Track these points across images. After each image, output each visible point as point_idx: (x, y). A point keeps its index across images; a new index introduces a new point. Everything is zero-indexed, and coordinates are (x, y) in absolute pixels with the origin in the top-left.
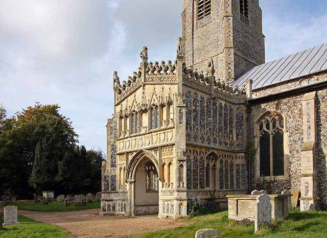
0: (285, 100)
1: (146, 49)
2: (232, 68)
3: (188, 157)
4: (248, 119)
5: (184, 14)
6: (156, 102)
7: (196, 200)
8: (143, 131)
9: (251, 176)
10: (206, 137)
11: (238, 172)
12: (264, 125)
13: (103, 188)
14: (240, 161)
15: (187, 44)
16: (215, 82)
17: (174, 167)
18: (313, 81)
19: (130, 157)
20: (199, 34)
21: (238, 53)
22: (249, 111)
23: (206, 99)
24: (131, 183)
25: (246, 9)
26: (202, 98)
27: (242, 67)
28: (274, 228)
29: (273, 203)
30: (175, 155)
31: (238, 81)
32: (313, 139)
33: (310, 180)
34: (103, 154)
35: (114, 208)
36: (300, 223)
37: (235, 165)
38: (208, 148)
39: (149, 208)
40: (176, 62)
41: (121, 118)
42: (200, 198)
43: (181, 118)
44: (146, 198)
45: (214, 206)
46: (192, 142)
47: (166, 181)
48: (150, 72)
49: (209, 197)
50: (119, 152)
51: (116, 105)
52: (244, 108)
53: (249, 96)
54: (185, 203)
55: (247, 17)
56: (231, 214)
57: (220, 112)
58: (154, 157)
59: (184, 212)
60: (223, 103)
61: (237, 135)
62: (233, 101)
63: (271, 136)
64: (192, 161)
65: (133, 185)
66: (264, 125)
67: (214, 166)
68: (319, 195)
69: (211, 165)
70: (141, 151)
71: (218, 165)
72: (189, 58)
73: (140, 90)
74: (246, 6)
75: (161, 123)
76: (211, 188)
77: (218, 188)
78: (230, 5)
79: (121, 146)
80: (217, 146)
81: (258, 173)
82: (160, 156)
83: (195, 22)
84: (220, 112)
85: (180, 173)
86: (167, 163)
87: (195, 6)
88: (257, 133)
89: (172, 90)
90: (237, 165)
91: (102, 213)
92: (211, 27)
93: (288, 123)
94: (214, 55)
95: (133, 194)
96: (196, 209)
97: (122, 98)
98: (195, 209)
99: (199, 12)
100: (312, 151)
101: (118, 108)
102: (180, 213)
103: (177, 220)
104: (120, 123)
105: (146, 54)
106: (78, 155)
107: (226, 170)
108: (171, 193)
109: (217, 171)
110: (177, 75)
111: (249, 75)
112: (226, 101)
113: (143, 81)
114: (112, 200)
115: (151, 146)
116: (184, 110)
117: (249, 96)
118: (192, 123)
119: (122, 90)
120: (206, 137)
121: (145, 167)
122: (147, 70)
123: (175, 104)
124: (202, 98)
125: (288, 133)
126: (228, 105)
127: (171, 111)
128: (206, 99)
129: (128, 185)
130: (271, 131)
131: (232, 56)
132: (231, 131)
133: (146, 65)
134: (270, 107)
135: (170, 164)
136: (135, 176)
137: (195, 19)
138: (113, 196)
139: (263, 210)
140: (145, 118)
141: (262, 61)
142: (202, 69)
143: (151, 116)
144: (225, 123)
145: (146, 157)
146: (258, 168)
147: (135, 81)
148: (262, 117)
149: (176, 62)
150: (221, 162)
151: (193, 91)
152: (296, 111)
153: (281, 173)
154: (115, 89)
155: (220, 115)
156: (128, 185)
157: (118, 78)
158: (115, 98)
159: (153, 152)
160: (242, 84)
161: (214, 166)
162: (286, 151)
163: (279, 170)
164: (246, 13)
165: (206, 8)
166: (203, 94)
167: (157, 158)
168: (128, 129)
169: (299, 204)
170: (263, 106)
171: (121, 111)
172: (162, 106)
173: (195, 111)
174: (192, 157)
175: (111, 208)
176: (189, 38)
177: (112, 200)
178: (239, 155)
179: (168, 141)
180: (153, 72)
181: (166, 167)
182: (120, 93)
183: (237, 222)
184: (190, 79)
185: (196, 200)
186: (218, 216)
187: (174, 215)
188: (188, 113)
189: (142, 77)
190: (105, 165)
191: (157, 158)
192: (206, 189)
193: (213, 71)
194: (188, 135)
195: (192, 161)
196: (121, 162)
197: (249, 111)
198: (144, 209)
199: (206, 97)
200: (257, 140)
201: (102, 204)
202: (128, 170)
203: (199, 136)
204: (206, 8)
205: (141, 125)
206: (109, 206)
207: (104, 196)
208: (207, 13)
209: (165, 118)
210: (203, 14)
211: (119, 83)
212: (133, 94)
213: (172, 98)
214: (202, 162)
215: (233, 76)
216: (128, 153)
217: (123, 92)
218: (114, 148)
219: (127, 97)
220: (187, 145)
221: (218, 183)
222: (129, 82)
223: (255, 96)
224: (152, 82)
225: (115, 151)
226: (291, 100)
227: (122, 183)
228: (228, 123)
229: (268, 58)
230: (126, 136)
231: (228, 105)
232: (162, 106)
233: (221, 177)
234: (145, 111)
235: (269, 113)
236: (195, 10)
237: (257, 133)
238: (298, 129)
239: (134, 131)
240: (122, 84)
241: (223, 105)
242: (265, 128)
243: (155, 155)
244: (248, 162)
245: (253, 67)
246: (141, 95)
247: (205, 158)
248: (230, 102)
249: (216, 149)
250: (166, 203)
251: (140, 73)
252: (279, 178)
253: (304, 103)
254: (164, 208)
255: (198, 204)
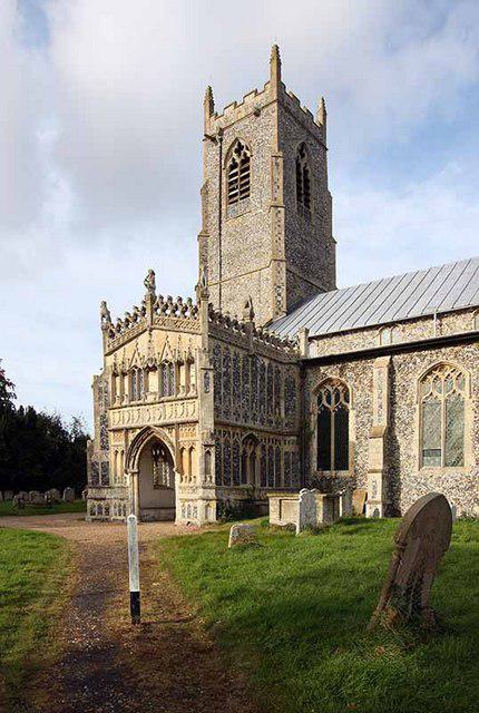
0: (352, 365)
1: (153, 273)
2: (284, 294)
3: (218, 439)
4: (302, 386)
5: (205, 191)
6: (170, 357)
7: (228, 500)
8: (150, 399)
9: (305, 470)
10: (241, 412)
11: (286, 463)
12: (324, 398)
13: (90, 481)
14: (289, 447)
15: (210, 244)
16: (254, 331)
17: (198, 454)
18: (386, 339)
19: (131, 437)
20: (231, 230)
21: (293, 268)
22: (303, 376)
23: (241, 356)
24: (133, 474)
25: (307, 194)
26: (237, 355)
27: (299, 292)
28: (317, 531)
29: (321, 504)
30: (198, 437)
31: (292, 316)
32: (384, 423)
33: (378, 477)
34: (62, 420)
35: (107, 510)
36: (351, 528)
37: (282, 453)
38: (245, 429)
39: (159, 508)
40: (199, 302)
41: (115, 375)
42: (233, 498)
43: (207, 385)
44: (155, 497)
45: (253, 508)
46: (223, 419)
47: (186, 474)
48: (159, 311)
49: (246, 497)
50: (113, 427)
51: (106, 355)
52: (296, 370)
53: (303, 354)
54: (214, 504)
55: (309, 207)
56: (273, 518)
57: (262, 376)
58: (169, 438)
59: (212, 517)
60: (267, 362)
61: (287, 410)
62: (280, 358)
63: (333, 414)
64: (223, 446)
65: (136, 478)
66: (324, 398)
67: (253, 452)
68: (390, 498)
69: (249, 452)
70: (149, 428)
71: (259, 453)
72: (214, 269)
73: (145, 337)
74: (307, 187)
75: (178, 388)
76: (248, 485)
77: (258, 485)
78: (281, 187)
79: (115, 419)
80: (258, 425)
81: (315, 465)
82: (177, 437)
83: (224, 207)
84: (262, 376)
85: (207, 463)
86: (187, 448)
87: (224, 180)
88: (314, 408)
89: (193, 342)
90: (286, 453)
91: (89, 517)
92: (250, 219)
93: (357, 397)
94: (254, 291)
95: (136, 491)
96: (227, 513)
97: (116, 345)
98: (228, 512)
99: (231, 191)
100: (381, 439)
101: (110, 359)
102: (206, 517)
103: (203, 526)
104: (114, 383)
105: (154, 282)
106: (24, 422)
107: (270, 459)
108: (194, 490)
109: (258, 465)
110: (200, 321)
111: (310, 308)
112: (270, 359)
113: (149, 322)
114: (104, 499)
115: (160, 422)
116: (211, 374)
117: (303, 354)
118: (223, 391)
119: (115, 332)
120: (241, 412)
121: (152, 451)
122: (155, 306)
123: (198, 365)
124: (237, 355)
125: (355, 412)
126: (274, 365)
127: (192, 373)
128: (241, 356)
129: (128, 476)
130: (332, 407)
131: (284, 275)
132: (278, 404)
133: (153, 299)
134: (331, 372)
135: (191, 449)
136: (138, 465)
137: (223, 202)
138: (105, 493)
139: (307, 510)
140: (154, 379)
141: (329, 285)
142: (234, 310)
143: (162, 376)
144: (270, 392)
145: (155, 437)
146: (315, 459)
147: (135, 320)
148: (321, 386)
149: (199, 302)
150: (263, 447)
151: (223, 346)
152: (366, 382)
153: (346, 467)
154: (104, 329)
155: (262, 379)
156: (128, 476)
157: (109, 312)
158: (105, 343)
159: (166, 431)
160: (289, 330)
161: (253, 452)
162: (352, 437)
163: (343, 463)
164: (307, 201)
165: (242, 186)
166: (238, 350)
167: (173, 440)
168: (127, 392)
169: (364, 511)
170: (322, 369)
171: (115, 365)
172: (179, 364)
173: (226, 374)
174: (222, 440)
175: (104, 510)
176: (214, 232)
177: (104, 499)
178: (288, 439)
179: (189, 417)
180: (164, 311)
181: (185, 453)
182: (112, 336)
183: (280, 527)
184: (219, 326)
185: (228, 500)
186: (258, 521)
187: (198, 520)
188: (217, 377)
189: (148, 315)
190: (92, 447)
191: (173, 440)
192: (242, 486)
193: (252, 315)
194: (216, 409)
195: (223, 446)
196: (118, 443)
197: (303, 376)
198: (152, 513)
199: (242, 354)
200: (314, 418)
201: (89, 505)
202: (129, 456)
203: (233, 411)
204: (242, 186)
205: (147, 390)
206: (100, 507)
207: (91, 492)
208: (244, 195)
209: (183, 382)
210: (236, 194)
211: (109, 319)
212: (133, 341)
213: (193, 355)
214: (236, 448)
215: (284, 309)
216: (127, 430)
217: (118, 335)
218: (104, 421)
219: (123, 345)
220: (216, 423)
221: (258, 478)
222: (127, 320)
223: (315, 352)
224: (163, 327)
225: (107, 426)
226: (361, 364)
227: (119, 474)
228: (273, 390)
229: (342, 281)
230: (124, 404)
231: (274, 365)
232: (179, 364)
233: (263, 469)
234: (154, 369)
235: (330, 380)
236: (224, 187)
237: (314, 408)
238: (367, 406)
239: (136, 397)
240: (115, 322)
241: (266, 364)
242: (342, 399)
243: (169, 435)
244: (301, 449)
245: (315, 294)
246: (146, 345)
247: (240, 443)
248: (275, 360)
249: (257, 430)
250: (186, 504)
251: (144, 309)
252: (343, 473)
253: (375, 371)
254: (183, 511)
255: (231, 507)
